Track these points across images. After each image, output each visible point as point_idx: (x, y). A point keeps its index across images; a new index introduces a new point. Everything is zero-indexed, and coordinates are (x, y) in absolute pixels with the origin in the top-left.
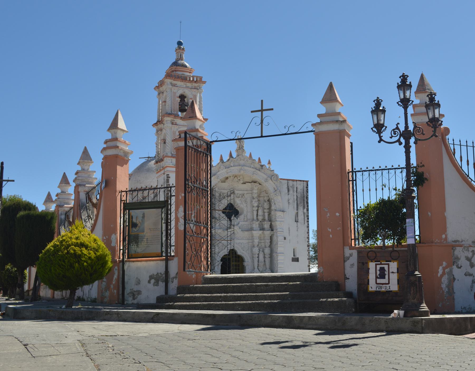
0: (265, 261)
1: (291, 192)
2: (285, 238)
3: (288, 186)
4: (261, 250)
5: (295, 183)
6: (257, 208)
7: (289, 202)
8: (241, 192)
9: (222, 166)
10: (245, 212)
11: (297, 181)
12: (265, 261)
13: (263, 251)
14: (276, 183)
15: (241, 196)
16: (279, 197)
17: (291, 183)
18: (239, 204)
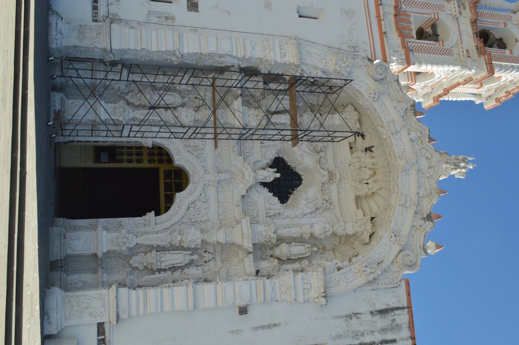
0: (160, 270)
1: (381, 322)
2: (243, 311)
3: (392, 310)
4: (195, 257)
5: (406, 333)
6: (307, 236)
7: (350, 317)
8: (334, 198)
9: (404, 106)
10: (288, 213)
11: (413, 338)
12: (160, 270)
13: (191, 263)
14: (394, 268)
15: (327, 197)
16: (361, 280)
17: (402, 318)
18: (304, 196)
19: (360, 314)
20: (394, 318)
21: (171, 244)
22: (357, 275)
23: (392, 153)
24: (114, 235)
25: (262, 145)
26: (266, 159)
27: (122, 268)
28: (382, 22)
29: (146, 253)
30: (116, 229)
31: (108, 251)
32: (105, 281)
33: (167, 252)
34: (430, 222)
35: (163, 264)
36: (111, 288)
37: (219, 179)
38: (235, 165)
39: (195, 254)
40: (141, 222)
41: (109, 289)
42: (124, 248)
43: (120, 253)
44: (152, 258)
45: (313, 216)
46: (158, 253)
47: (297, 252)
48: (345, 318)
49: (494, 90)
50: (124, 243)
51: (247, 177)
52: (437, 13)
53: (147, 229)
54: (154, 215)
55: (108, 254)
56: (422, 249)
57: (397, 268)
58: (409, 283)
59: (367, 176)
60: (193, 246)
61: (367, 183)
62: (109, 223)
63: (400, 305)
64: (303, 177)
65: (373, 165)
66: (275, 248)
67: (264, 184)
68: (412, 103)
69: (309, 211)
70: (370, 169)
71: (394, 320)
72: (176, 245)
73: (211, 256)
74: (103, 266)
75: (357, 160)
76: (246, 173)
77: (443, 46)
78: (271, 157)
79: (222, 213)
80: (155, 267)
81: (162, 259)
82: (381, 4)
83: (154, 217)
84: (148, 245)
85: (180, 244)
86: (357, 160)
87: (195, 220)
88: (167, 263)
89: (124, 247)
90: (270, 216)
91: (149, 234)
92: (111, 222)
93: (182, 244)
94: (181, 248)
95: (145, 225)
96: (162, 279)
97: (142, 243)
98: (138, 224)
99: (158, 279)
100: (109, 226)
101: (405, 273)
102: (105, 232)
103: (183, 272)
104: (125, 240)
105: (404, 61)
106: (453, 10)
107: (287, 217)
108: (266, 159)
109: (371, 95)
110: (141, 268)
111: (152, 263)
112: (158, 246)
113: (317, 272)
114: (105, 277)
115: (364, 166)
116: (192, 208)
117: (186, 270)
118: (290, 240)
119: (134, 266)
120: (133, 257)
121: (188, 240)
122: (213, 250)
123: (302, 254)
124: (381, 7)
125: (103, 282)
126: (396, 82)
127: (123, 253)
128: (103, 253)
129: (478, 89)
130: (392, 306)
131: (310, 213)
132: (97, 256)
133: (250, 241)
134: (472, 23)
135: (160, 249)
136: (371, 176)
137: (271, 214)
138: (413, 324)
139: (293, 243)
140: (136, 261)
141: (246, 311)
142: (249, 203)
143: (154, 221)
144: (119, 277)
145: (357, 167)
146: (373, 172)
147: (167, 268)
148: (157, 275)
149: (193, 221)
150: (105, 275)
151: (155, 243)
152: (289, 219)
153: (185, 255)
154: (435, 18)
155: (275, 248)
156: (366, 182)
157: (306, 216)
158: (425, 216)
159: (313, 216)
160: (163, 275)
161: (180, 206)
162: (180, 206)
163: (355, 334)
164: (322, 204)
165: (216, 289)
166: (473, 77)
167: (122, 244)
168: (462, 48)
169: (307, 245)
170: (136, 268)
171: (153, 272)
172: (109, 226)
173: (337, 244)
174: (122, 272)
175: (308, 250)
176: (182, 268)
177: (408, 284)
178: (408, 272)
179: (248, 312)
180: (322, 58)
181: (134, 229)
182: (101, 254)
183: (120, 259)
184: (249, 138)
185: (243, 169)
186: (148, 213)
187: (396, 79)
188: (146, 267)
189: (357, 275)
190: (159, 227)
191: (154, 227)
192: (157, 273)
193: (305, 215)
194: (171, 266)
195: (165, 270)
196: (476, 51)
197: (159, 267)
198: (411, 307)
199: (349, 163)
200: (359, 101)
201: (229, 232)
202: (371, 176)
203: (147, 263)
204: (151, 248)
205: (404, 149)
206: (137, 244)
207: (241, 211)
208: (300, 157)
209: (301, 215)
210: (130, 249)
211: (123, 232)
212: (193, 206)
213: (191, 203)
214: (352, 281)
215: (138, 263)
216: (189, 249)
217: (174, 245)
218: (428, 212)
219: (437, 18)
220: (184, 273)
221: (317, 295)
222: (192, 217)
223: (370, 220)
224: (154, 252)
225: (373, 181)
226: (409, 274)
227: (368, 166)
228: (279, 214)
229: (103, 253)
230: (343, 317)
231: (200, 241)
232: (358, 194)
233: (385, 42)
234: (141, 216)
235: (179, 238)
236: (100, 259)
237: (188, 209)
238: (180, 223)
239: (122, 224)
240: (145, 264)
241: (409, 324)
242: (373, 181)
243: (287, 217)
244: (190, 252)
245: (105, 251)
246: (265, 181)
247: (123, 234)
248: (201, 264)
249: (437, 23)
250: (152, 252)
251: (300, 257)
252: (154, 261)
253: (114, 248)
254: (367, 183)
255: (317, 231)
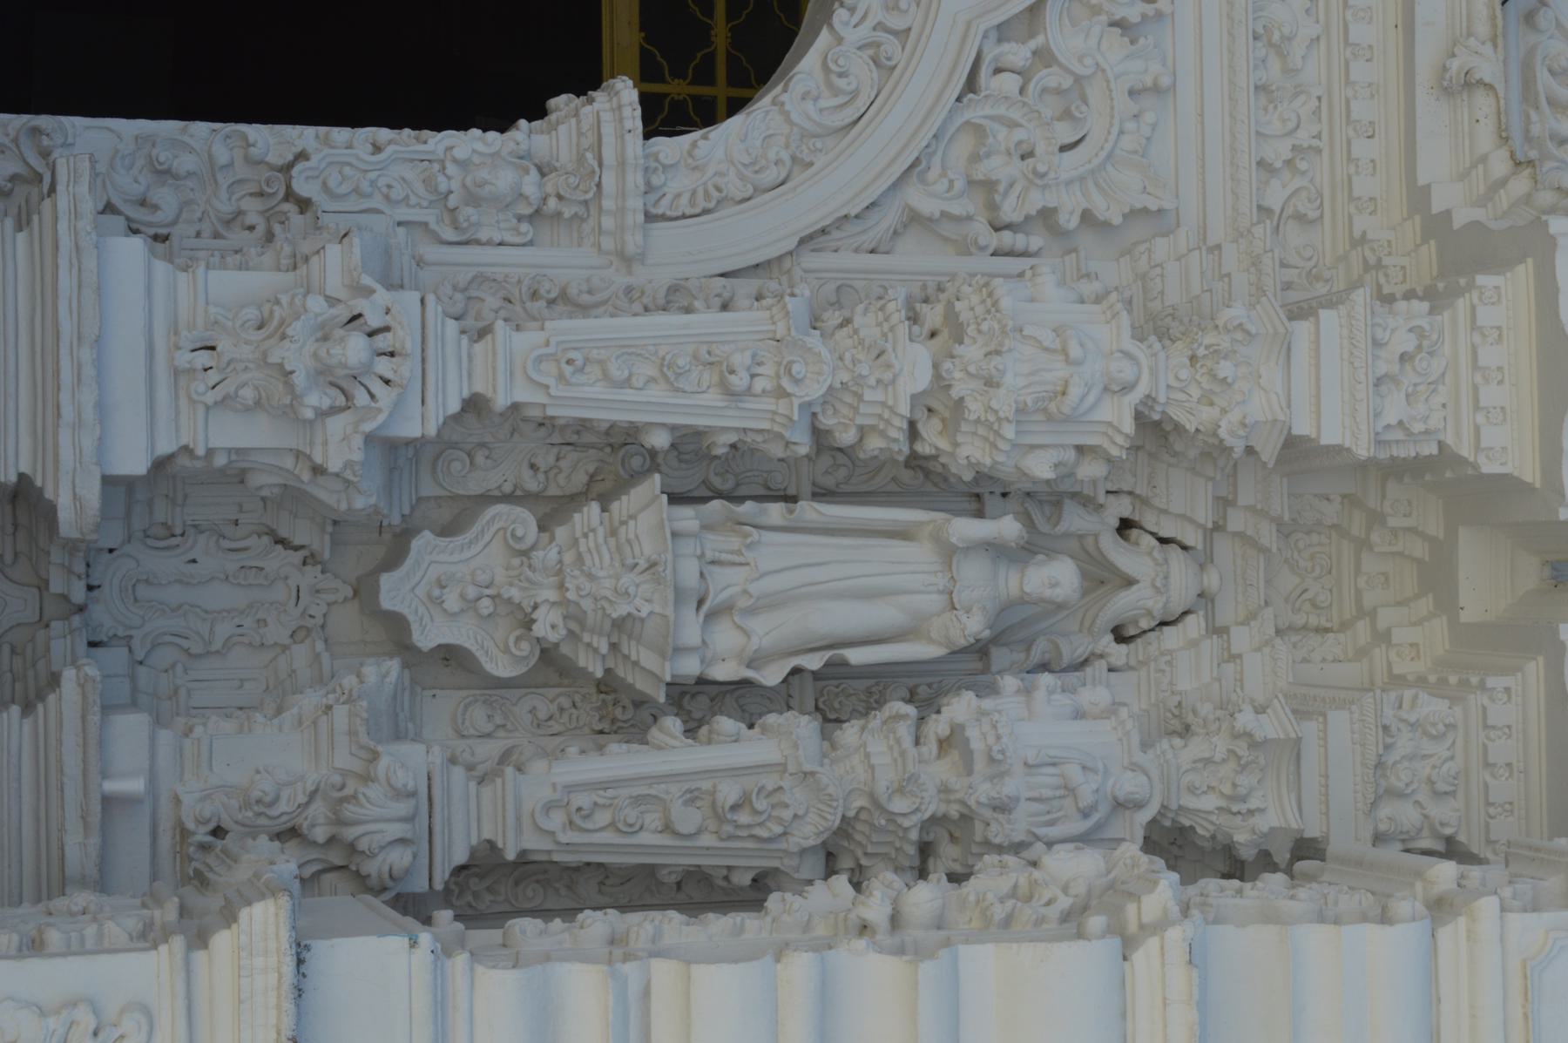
0: (699, 701)
4: (1056, 577)
12: (699, 701)
21: (819, 435)
24: (234, 286)
27: (301, 654)
29: (553, 510)
30: (237, 237)
31: (161, 465)
32: (129, 801)
33: (775, 512)
35: (725, 637)
36: (222, 940)
39: (1051, 553)
40: (504, 180)
41: (200, 940)
42: (340, 445)
43: (292, 497)
44: (631, 566)
46: (687, 517)
50: (344, 386)
53: (561, 260)
54: (634, 118)
55: (158, 498)
60: (1041, 467)
62: (164, 174)
72: (874, 444)
73: (1181, 578)
74: (106, 615)
80: (648, 660)
81: (726, 584)
83: (635, 141)
84: (583, 425)
85: (913, 432)
87: (1036, 201)
88: (767, 630)
89: (337, 425)
91: (584, 310)
92: (185, 163)
93: (933, 438)
94: (920, 479)
95: (536, 216)
96: (729, 792)
97: (522, 394)
98: (473, 199)
99: (692, 798)
100: (167, 199)
102: (132, 249)
103: (938, 726)
104: (355, 348)
110: (502, 668)
111: (619, 624)
112: (689, 444)
114: (133, 755)
116: (1009, 82)
117: (960, 708)
119: (427, 637)
120: (423, 542)
121: (1003, 402)
122: (1205, 515)
125: (108, 801)
127: (325, 493)
128: (108, 481)
132: (49, 512)
135: (711, 475)
140: (448, 586)
142: (1543, 76)
143: (635, 180)
144: (271, 758)
147: (772, 676)
148: (670, 754)
149: (1010, 211)
150: (130, 728)
151: (658, 408)
153: (949, 553)
160: (736, 750)
161: (891, 45)
162: (891, 45)
167: (316, 399)
170: (450, 655)
171: (620, 711)
172: (167, 199)
174: (310, 701)
176: (923, 687)
181: (432, 252)
182: (92, 493)
183: (279, 560)
186: (561, 103)
188: (548, 655)
190: (678, 252)
191: (633, 242)
192: (673, 724)
194: (814, 662)
195: (743, 698)
197: (690, 667)
201: (1408, 343)
203: (574, 616)
204: (613, 459)
206: (474, 405)
210: (393, 453)
211: (335, 265)
212: (1017, 53)
213: (1003, 32)
215: (471, 604)
216: (979, 495)
217: (847, 437)
220: (944, 744)
222: (998, 167)
224: (644, 505)
229: (108, 481)
231: (1120, 415)
234: (501, 122)
235: (914, 367)
236: (71, 546)
237: (971, 85)
238: (890, 217)
239: (302, 188)
240: (548, 625)
244: (1007, 527)
245: (134, 463)
247: (335, 285)
248: (1081, 651)
250: (620, 507)
252: (646, 602)
253: (230, 434)
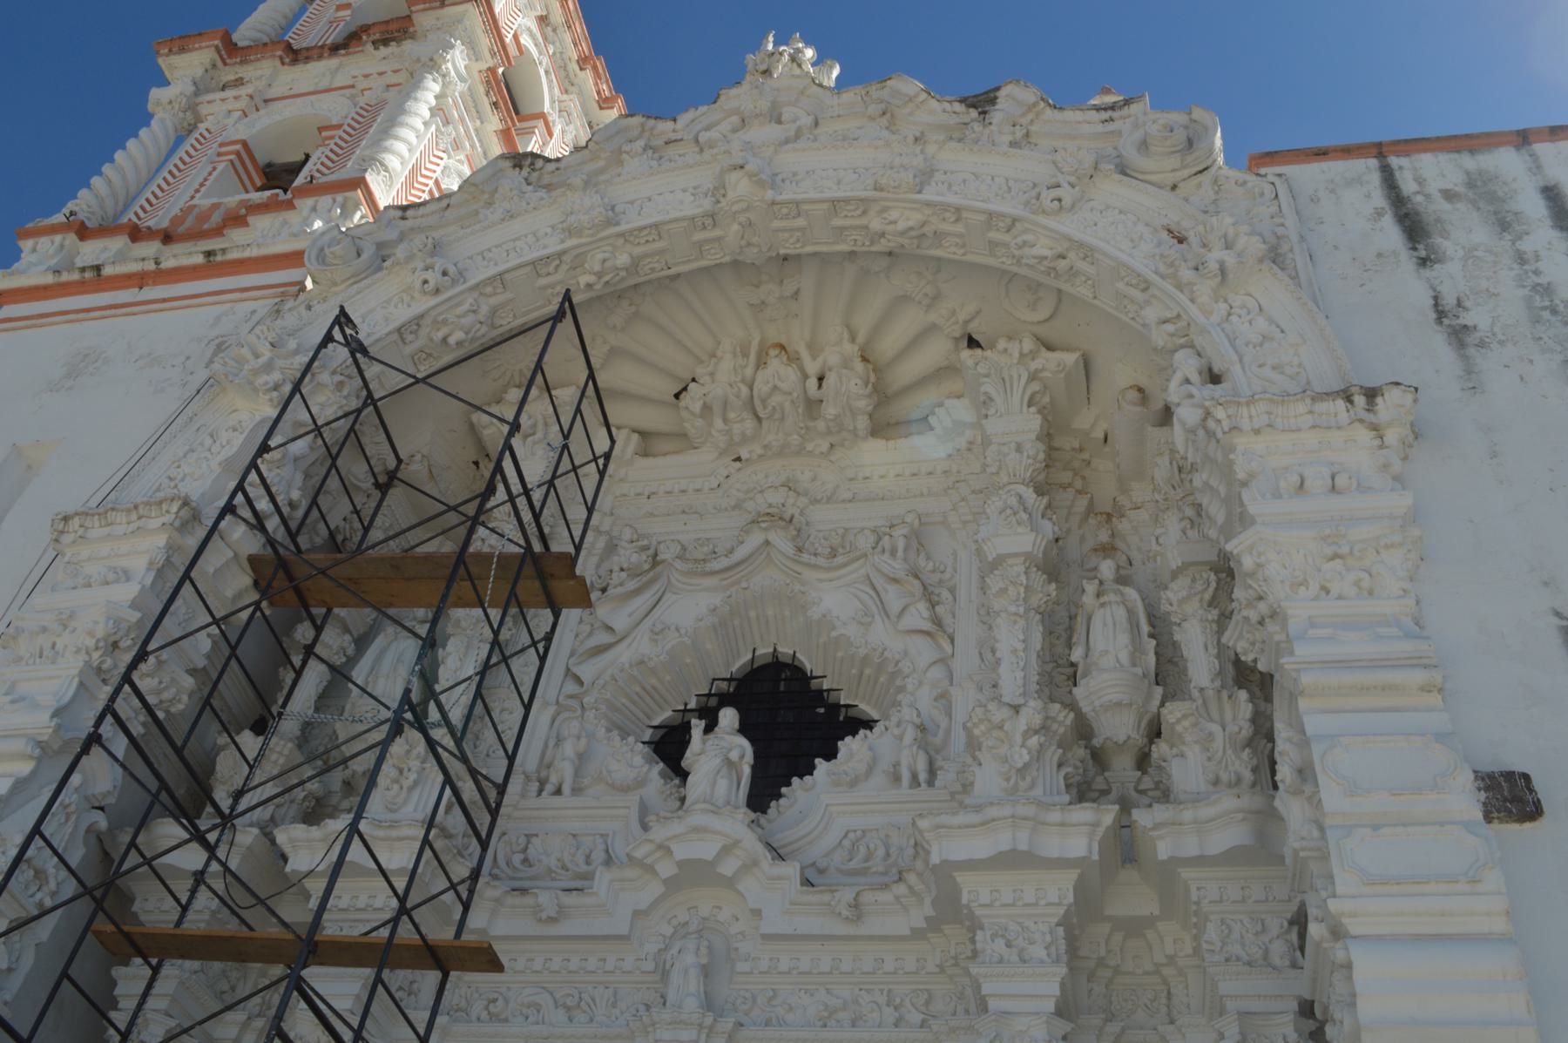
10: (920, 699)
15: (865, 542)
19: (1436, 298)
20: (1437, 196)
22: (1244, 306)
23: (699, 236)
25: (566, 789)
26: (640, 783)
28: (163, 266)
34: (1002, 93)
37: (691, 1004)
38: (637, 914)
45: (945, 594)
47: (1124, 639)
48: (1472, 351)
49: (565, 97)
51: (706, 850)
52: (221, 145)
56: (1115, 114)
57: (1199, 186)
58: (1269, 154)
59: (790, 375)
61: (821, 379)
63: (1375, 179)
64: (764, 650)
65: (745, 355)
66: (1096, 742)
67: (762, 795)
68: (508, 164)
69: (922, 607)
70: (761, 363)
71: (1449, 195)
75: (718, 423)
76: (681, 852)
77: (339, 127)
78: (638, 760)
79: (888, 1011)
82: (98, 268)
86: (718, 423)
90: (932, 772)
101: (1221, 160)
105: (340, 198)
106: (231, 105)
107: (943, 697)
108: (640, 783)
109: (432, 284)
113: (1235, 428)
115: (745, 390)
118: (1060, 673)
123: (1134, 626)
124: (108, 271)
126: (409, 213)
129: (551, 134)
130: (1379, 199)
131: (933, 605)
133: (1055, 816)
134: (295, 61)
136: (793, 359)
137: (922, 766)
138: (1455, 137)
139: (1077, 655)
141: (1509, 776)
142: (853, 865)
145: (750, 424)
146: (773, 352)
152: (954, 691)
154: (238, 154)
155: (1096, 742)
156: (812, 383)
157: (947, 620)
158: (974, 113)
159: (945, 594)
163: (1546, 314)
164: (893, 552)
165: (1380, 938)
166: (484, 66)
168: (366, 76)
169: (1088, 599)
173: (1082, 503)
175: (1112, 597)
177: (1271, 157)
178: (1218, 142)
179: (1519, 767)
180: (208, 441)
184: (492, 795)
185: (666, 869)
187: (399, 213)
189: (1244, 306)
193: (938, 622)
196: (393, 48)
198: (1379, 145)
199: (728, 460)
200: (452, 340)
201: (1000, 942)
202: (793, 359)
205: (684, 191)
207: (886, 897)
208: (656, 633)
209: (944, 669)
214: (1271, 321)
218: (958, 107)
219: (238, 147)
221: (1364, 436)
223: (979, 351)
225: (814, 357)
226: (1223, 137)
227: (749, 372)
228: (922, 728)
230: (1465, 358)
232: (862, 423)
233: (247, 254)
241: (1458, 151)
242: (814, 357)
243: (943, 697)
246: (747, 771)
249: (262, 159)
251: (1145, 628)
254: (821, 379)
255: (1021, 541)
